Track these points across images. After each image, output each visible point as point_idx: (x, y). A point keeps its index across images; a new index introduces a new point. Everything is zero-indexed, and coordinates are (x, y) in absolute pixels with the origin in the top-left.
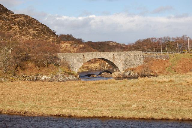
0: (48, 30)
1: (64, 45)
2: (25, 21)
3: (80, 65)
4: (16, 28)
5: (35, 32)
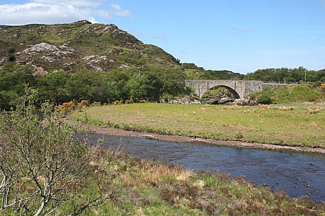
0: (173, 59)
1: (188, 72)
2: (153, 50)
3: (205, 91)
4: (145, 56)
5: (162, 60)
